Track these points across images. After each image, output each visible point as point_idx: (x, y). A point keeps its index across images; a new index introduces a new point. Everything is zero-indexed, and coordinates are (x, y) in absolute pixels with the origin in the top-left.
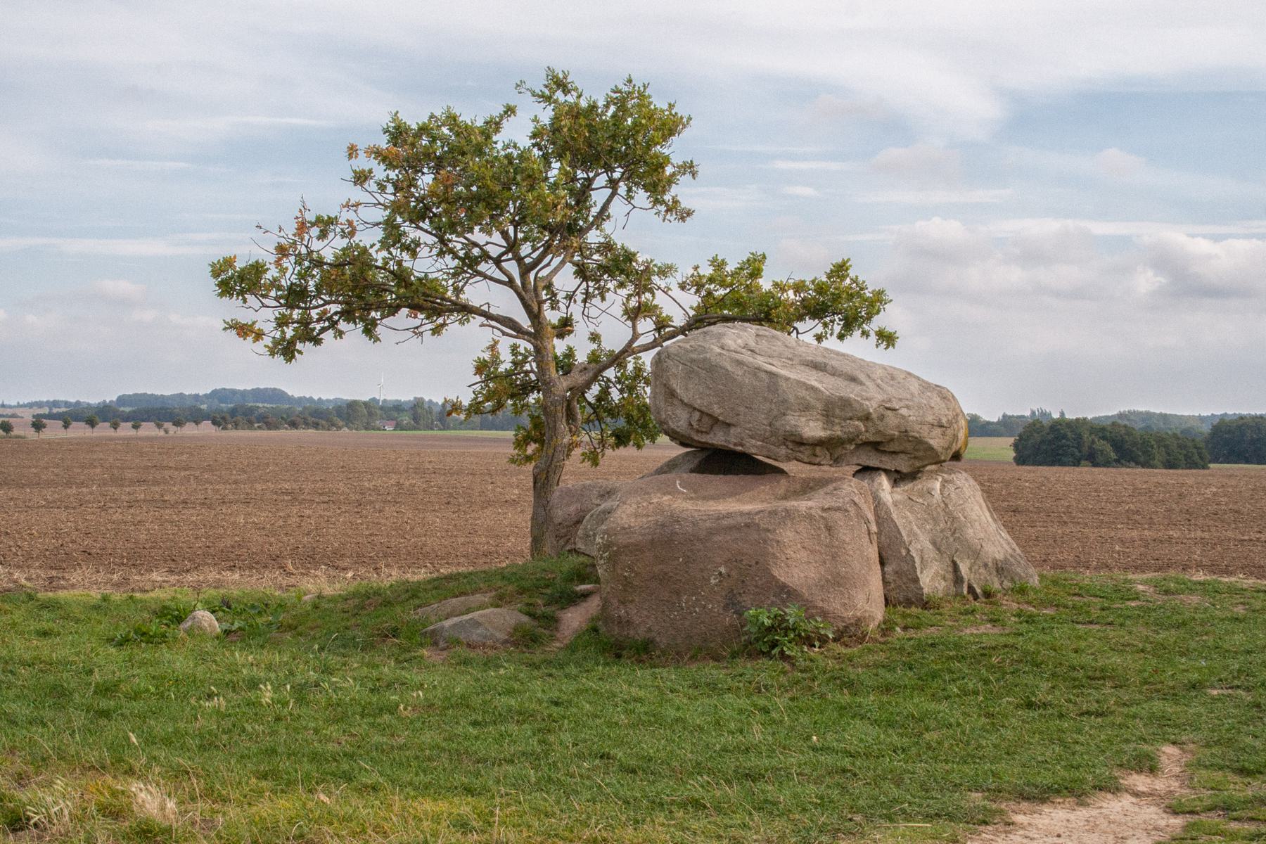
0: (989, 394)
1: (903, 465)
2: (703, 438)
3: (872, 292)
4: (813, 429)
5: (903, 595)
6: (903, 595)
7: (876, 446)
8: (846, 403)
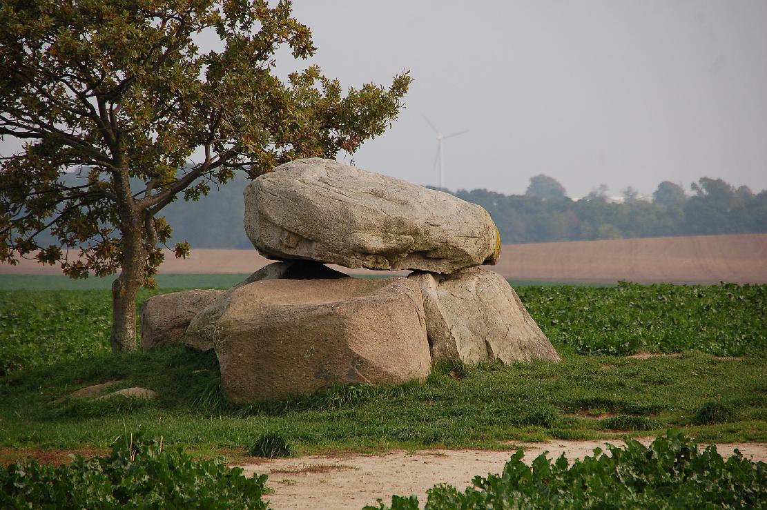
1: (444, 268)
4: (375, 242)
6: (449, 366)
7: (424, 255)
8: (400, 223)
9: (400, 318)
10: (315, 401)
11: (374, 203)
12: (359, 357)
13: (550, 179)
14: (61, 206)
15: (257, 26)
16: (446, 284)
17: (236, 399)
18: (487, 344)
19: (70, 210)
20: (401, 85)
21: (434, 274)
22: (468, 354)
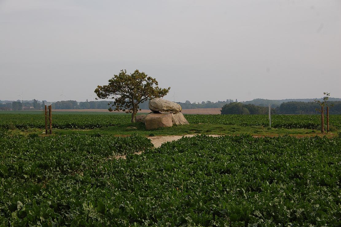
4: (165, 109)
5: (175, 125)
6: (175, 125)
7: (172, 111)
10: (158, 129)
11: (165, 104)
20: (169, 88)
22: (177, 123)
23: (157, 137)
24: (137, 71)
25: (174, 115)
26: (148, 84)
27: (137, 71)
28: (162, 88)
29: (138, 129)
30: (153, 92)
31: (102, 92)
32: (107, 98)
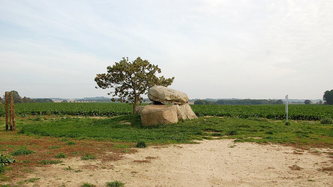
0: (194, 95)
1: (180, 103)
2: (155, 100)
3: (324, 100)
4: (169, 99)
5: (181, 120)
6: (181, 120)
7: (177, 101)
8: (173, 95)
9: (173, 112)
10: (157, 127)
11: (169, 92)
12: (165, 119)
13: (45, 100)
14: (129, 95)
15: (153, 69)
16: (180, 106)
17: (144, 125)
18: (187, 116)
19: (130, 96)
20: (173, 78)
21: (178, 104)
22: (184, 118)
23: (156, 146)
24: (139, 58)
25: (180, 107)
26: (152, 73)
27: (139, 58)
28: (166, 78)
29: (132, 125)
30: (156, 82)
31: (102, 81)
32: (108, 87)
